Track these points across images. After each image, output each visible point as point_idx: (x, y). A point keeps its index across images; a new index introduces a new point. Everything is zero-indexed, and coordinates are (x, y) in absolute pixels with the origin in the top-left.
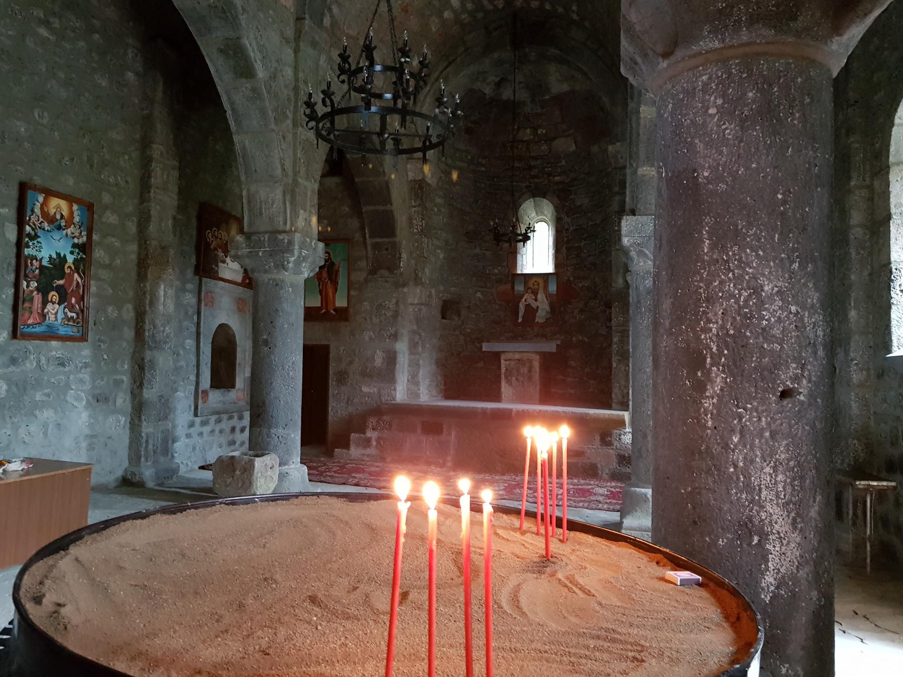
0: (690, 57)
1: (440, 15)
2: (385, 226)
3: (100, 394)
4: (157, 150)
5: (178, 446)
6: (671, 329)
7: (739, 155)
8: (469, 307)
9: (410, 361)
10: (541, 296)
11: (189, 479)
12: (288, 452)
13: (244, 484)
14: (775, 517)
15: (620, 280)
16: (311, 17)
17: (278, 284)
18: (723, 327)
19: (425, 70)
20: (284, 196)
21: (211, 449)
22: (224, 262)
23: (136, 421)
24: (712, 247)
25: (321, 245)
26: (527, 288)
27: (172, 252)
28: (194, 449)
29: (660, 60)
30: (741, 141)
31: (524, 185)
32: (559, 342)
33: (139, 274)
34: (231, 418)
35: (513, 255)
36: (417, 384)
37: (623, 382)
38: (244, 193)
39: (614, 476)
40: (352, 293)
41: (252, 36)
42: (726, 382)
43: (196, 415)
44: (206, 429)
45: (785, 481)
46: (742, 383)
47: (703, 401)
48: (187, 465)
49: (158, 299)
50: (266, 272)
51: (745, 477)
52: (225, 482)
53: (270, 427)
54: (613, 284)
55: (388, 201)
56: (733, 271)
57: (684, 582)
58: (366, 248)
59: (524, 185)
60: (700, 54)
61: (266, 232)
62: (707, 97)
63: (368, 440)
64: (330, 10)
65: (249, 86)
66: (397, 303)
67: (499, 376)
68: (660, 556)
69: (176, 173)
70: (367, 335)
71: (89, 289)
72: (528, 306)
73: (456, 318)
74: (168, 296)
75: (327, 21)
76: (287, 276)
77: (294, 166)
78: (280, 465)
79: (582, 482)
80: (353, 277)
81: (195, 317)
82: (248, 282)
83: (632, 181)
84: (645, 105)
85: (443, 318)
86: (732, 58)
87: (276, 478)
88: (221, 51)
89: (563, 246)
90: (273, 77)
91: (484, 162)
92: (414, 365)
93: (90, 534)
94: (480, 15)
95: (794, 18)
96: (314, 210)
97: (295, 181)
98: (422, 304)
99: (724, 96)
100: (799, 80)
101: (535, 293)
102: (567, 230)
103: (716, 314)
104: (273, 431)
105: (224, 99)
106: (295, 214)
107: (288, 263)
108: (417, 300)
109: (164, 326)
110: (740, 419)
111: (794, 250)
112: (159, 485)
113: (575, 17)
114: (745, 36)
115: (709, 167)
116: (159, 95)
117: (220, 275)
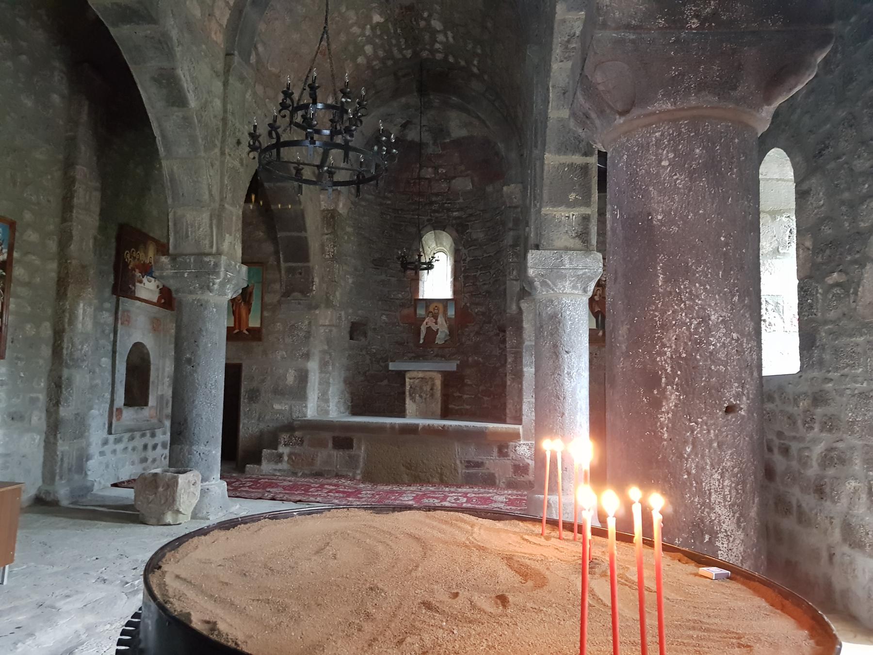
0: (646, 116)
1: (354, 58)
2: (299, 251)
3: (15, 413)
4: (82, 171)
5: (92, 464)
6: (627, 352)
7: (689, 202)
8: (375, 329)
9: (321, 379)
10: (441, 320)
11: (103, 497)
12: (209, 468)
13: (167, 500)
14: (723, 517)
15: (514, 307)
16: (239, 53)
17: (202, 305)
18: (676, 351)
19: (363, 110)
20: (211, 220)
21: (123, 466)
22: (141, 282)
23: (52, 440)
24: (666, 281)
25: (244, 268)
26: (428, 313)
27: (92, 272)
28: (107, 466)
29: (618, 117)
30: (690, 190)
31: (425, 218)
32: (458, 362)
33: (58, 292)
34: (143, 435)
35: (415, 281)
36: (327, 401)
37: (516, 399)
38: (171, 216)
39: (511, 485)
40: (266, 314)
41: (186, 68)
42: (679, 400)
43: (110, 433)
44: (120, 447)
45: (730, 486)
46: (693, 400)
47: (659, 416)
48: (100, 483)
49: (76, 318)
50: (191, 292)
51: (697, 483)
52: (148, 499)
53: (192, 444)
54: (508, 311)
55: (303, 228)
56: (684, 302)
57: (718, 577)
58: (280, 272)
59: (425, 218)
60: (654, 113)
61: (193, 255)
62: (660, 151)
63: (280, 456)
64: (256, 48)
65: (180, 114)
66: (310, 323)
67: (404, 393)
68: (679, 555)
69: (97, 195)
70: (280, 354)
71: (8, 306)
72: (429, 329)
73: (363, 340)
74: (87, 315)
75: (253, 59)
76: (211, 297)
77: (221, 192)
78: (203, 480)
79: (482, 490)
80: (266, 299)
81: (112, 336)
82: (167, 299)
83: (536, 219)
84: (549, 152)
85: (351, 338)
86: (681, 119)
87: (198, 494)
88: (154, 79)
89: (461, 274)
90: (204, 106)
91: (390, 195)
92: (325, 384)
93: (170, 551)
94: (390, 63)
95: (735, 88)
96: (239, 235)
97: (222, 207)
98: (333, 326)
99: (675, 151)
100: (736, 140)
101: (436, 317)
102: (465, 260)
103: (670, 340)
104: (194, 448)
105: (154, 125)
106: (221, 238)
107: (214, 284)
108: (328, 322)
109: (82, 344)
110: (692, 432)
111: (734, 285)
112: (72, 503)
113: (475, 70)
114: (693, 101)
115: (663, 212)
116: (84, 117)
117: (136, 295)
